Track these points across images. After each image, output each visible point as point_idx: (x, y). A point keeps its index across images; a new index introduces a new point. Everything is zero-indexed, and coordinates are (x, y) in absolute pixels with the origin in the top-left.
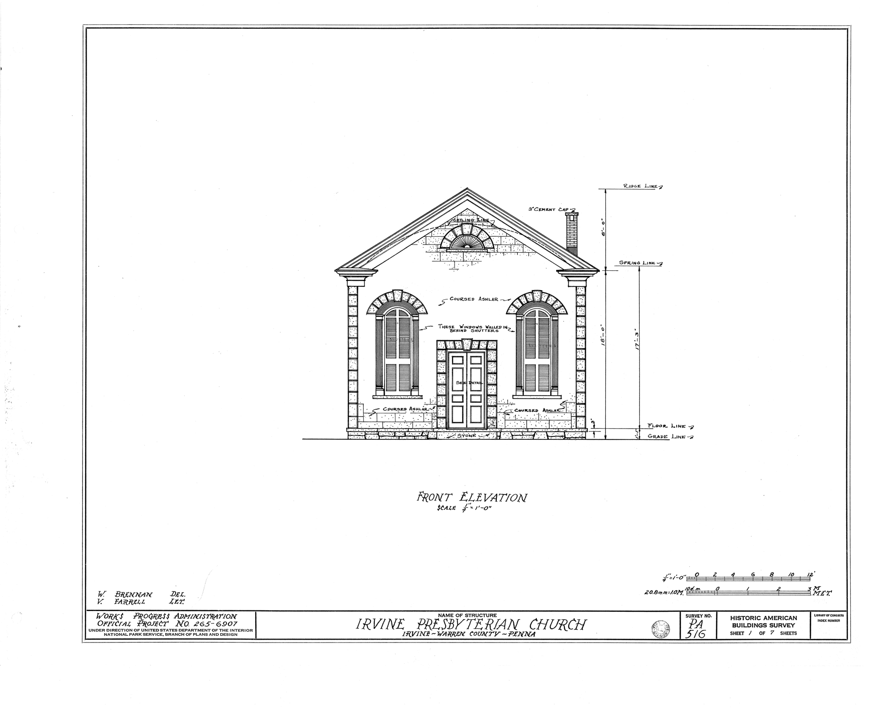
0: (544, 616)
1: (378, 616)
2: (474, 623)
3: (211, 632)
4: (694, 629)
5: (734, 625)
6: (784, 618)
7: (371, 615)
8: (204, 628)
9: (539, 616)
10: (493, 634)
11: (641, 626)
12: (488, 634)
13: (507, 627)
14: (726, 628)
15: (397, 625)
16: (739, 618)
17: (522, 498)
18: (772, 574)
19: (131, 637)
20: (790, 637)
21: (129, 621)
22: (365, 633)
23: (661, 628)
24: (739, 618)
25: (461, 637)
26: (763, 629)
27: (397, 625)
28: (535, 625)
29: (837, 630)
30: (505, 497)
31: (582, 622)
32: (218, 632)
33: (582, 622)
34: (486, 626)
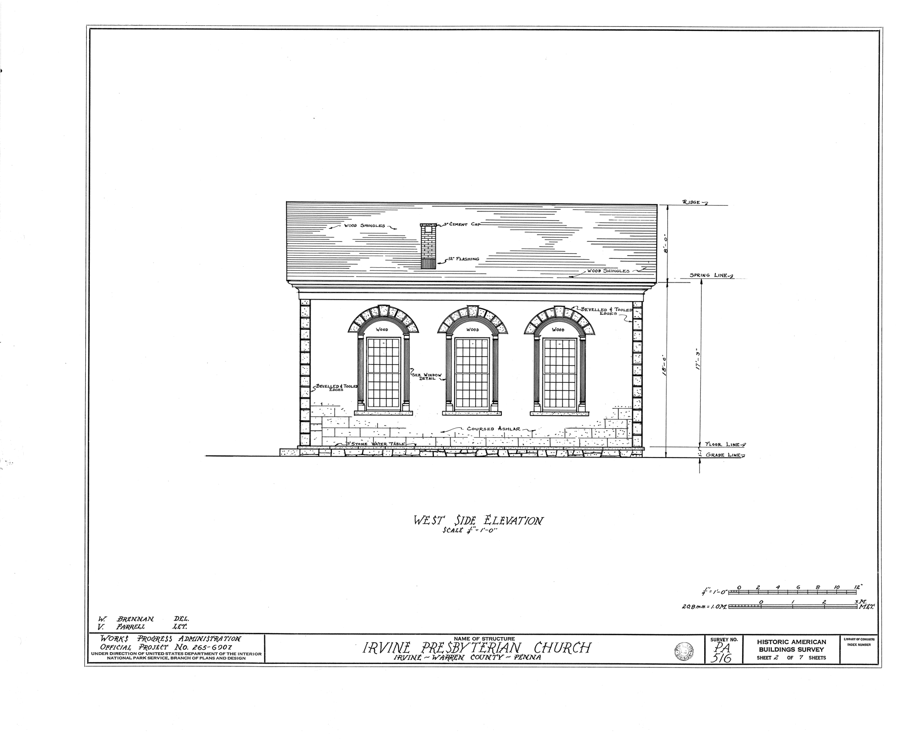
0: (549, 640)
1: (385, 639)
2: (479, 647)
3: (218, 655)
4: (720, 652)
5: (761, 650)
6: (813, 642)
7: (377, 639)
8: (201, 651)
9: (544, 639)
10: (497, 658)
11: (664, 650)
12: (492, 658)
13: (509, 650)
14: (752, 652)
15: (404, 648)
16: (766, 642)
17: (538, 521)
18: (818, 587)
19: (135, 660)
20: (818, 662)
21: (127, 644)
22: (371, 657)
23: (684, 650)
24: (766, 642)
25: (460, 661)
26: (791, 654)
27: (404, 648)
28: (540, 648)
29: (868, 654)
30: (524, 520)
31: (587, 645)
32: (226, 655)
33: (587, 645)
34: (496, 648)
